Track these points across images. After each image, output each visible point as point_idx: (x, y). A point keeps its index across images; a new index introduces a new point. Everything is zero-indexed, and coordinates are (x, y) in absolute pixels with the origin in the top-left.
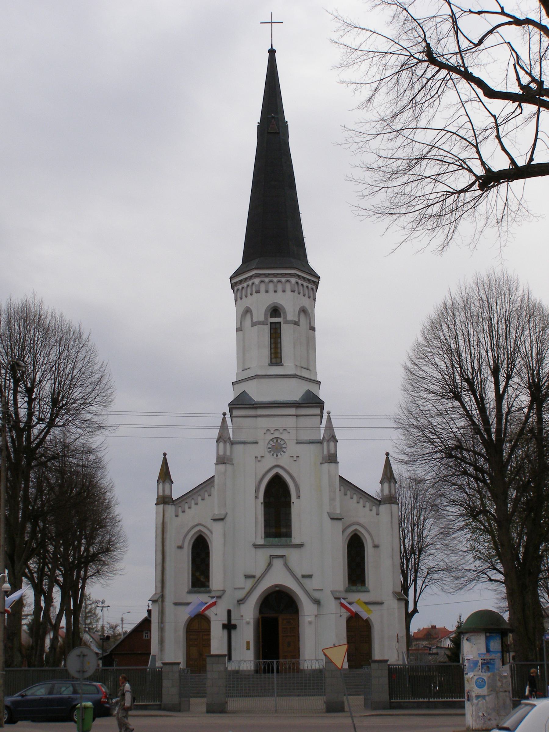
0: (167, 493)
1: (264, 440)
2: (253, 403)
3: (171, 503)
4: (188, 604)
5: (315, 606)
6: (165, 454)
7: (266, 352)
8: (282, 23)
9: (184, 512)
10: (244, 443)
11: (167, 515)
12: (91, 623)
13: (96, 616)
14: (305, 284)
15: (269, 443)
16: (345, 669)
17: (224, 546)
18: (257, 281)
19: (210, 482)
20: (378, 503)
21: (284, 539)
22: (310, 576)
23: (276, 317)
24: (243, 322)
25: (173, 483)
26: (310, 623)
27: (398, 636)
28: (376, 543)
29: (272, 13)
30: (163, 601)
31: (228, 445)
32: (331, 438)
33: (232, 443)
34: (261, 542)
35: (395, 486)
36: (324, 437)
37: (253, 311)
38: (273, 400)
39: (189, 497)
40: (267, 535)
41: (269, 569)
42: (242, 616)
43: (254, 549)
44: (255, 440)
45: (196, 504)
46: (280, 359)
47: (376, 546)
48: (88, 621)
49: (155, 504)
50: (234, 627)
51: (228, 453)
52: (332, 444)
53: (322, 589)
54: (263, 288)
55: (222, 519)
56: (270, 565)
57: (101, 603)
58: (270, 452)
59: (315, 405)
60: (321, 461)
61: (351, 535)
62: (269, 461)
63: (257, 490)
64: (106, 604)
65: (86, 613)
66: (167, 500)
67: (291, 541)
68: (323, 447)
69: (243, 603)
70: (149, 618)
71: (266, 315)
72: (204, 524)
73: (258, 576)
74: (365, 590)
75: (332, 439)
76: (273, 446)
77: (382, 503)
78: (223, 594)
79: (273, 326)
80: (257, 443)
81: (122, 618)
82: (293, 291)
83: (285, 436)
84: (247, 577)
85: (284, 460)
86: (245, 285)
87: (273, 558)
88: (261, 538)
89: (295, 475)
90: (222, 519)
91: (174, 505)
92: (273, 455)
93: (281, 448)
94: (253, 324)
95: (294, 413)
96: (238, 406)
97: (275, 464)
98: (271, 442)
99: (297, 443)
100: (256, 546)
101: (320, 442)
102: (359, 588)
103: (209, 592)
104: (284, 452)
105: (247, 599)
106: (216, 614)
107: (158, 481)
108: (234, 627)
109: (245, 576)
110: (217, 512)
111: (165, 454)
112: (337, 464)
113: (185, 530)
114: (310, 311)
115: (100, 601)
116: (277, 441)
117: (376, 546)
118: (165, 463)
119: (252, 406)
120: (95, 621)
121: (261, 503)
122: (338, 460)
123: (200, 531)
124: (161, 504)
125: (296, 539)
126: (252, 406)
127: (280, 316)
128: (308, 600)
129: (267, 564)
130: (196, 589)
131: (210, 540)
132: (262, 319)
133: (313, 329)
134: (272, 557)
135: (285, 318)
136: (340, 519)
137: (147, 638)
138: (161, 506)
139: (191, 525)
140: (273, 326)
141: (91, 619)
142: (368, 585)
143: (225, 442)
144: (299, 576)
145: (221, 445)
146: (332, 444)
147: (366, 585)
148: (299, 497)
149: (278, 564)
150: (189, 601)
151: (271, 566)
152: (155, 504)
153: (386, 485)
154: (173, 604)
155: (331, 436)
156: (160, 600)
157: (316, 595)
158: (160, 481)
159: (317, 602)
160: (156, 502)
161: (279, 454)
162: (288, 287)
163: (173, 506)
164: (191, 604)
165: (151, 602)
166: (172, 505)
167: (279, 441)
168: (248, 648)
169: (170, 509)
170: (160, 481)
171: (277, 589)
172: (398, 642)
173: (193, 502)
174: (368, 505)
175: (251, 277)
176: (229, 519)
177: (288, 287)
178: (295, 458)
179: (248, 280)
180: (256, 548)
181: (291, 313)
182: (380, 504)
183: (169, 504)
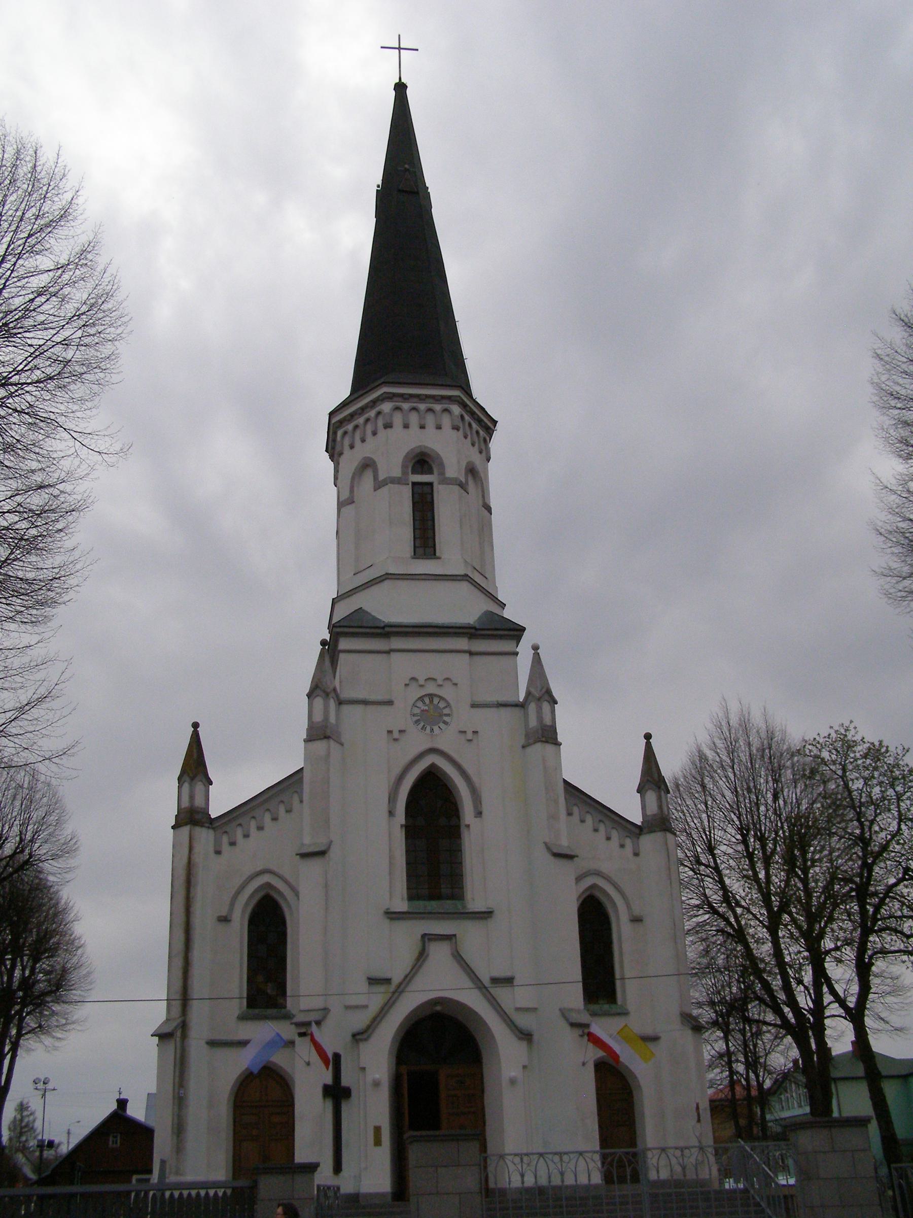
0: (199, 802)
1: (406, 699)
2: (382, 625)
3: (207, 825)
4: (243, 1043)
5: (524, 1045)
6: (196, 725)
7: (406, 534)
8: (417, 50)
9: (233, 844)
10: (365, 702)
11: (198, 849)
12: (27, 1141)
13: (35, 1131)
14: (474, 426)
15: (414, 705)
16: (596, 1187)
17: (327, 909)
18: (386, 407)
19: (294, 781)
20: (637, 831)
21: (448, 905)
22: (509, 981)
23: (422, 473)
24: (355, 489)
25: (211, 783)
26: (513, 1082)
27: (698, 1108)
28: (637, 912)
29: (399, 35)
30: (184, 1036)
31: (332, 704)
32: (543, 695)
33: (340, 703)
34: (401, 905)
35: (666, 798)
36: (528, 694)
37: (379, 466)
38: (424, 621)
39: (244, 813)
40: (412, 897)
41: (420, 966)
42: (363, 1069)
43: (388, 921)
44: (387, 697)
45: (260, 828)
46: (432, 549)
47: (637, 920)
48: (24, 1138)
49: (173, 827)
50: (346, 1093)
51: (332, 719)
52: (546, 707)
53: (536, 1009)
54: (398, 419)
55: (322, 853)
56: (422, 956)
57: (42, 1083)
58: (417, 722)
59: (506, 633)
60: (522, 741)
61: (584, 896)
62: (417, 741)
63: (392, 799)
64: (50, 1086)
65: (22, 1128)
66: (198, 817)
67: (464, 907)
68: (526, 715)
69: (366, 1040)
70: (120, 1112)
71: (404, 466)
72: (276, 869)
73: (397, 979)
74: (619, 1011)
75: (546, 697)
76: (423, 711)
77: (645, 831)
78: (324, 1017)
79: (418, 489)
80: (390, 703)
81: (69, 1130)
82: (456, 428)
83: (447, 692)
84: (373, 981)
85: (446, 739)
86: (361, 420)
87: (430, 940)
88: (402, 899)
89: (470, 771)
90: (322, 853)
91: (213, 829)
92: (424, 728)
93: (441, 715)
94: (379, 485)
95: (466, 648)
96: (351, 630)
97: (428, 745)
98: (420, 704)
99: (473, 706)
100: (392, 916)
101: (522, 706)
102: (606, 1007)
103: (288, 1017)
104: (445, 723)
105: (374, 1030)
106: (308, 1064)
107: (179, 779)
108: (346, 1093)
109: (369, 979)
110: (309, 842)
111: (196, 725)
112: (558, 747)
113: (237, 882)
114: (482, 475)
115: (40, 1080)
116: (431, 701)
117: (637, 920)
118: (195, 743)
119: (379, 631)
120: (32, 1138)
121: (402, 826)
122: (560, 739)
123: (268, 885)
124: (186, 824)
125: (475, 901)
126: (379, 631)
127: (430, 472)
128: (507, 1032)
129: (416, 954)
130: (257, 1011)
131: (289, 907)
132: (397, 472)
133: (489, 510)
134: (427, 938)
135: (442, 473)
136: (570, 857)
137: (115, 1146)
138: (185, 830)
139: (248, 870)
140: (418, 489)
141: (27, 1135)
142: (624, 999)
143: (327, 694)
144: (486, 981)
145: (319, 702)
146: (546, 707)
147: (619, 1002)
148: (479, 814)
149: (439, 953)
150: (242, 1035)
151: (424, 961)
152: (173, 827)
153: (651, 796)
154: (208, 1043)
155: (544, 690)
156: (179, 1033)
157: (523, 1021)
158: (186, 778)
159: (526, 1036)
160: (173, 823)
161: (436, 728)
162: (446, 421)
163: (211, 832)
164: (249, 1045)
165: (157, 1038)
166: (209, 827)
167: (436, 701)
168: (378, 1142)
169: (204, 837)
170: (186, 778)
171: (438, 1008)
172: (699, 1121)
173: (253, 824)
174: (615, 834)
175: (374, 403)
176: (334, 853)
177: (446, 421)
178: (470, 735)
179: (368, 410)
180: (391, 919)
181: (454, 469)
182: (640, 834)
183: (202, 826)
